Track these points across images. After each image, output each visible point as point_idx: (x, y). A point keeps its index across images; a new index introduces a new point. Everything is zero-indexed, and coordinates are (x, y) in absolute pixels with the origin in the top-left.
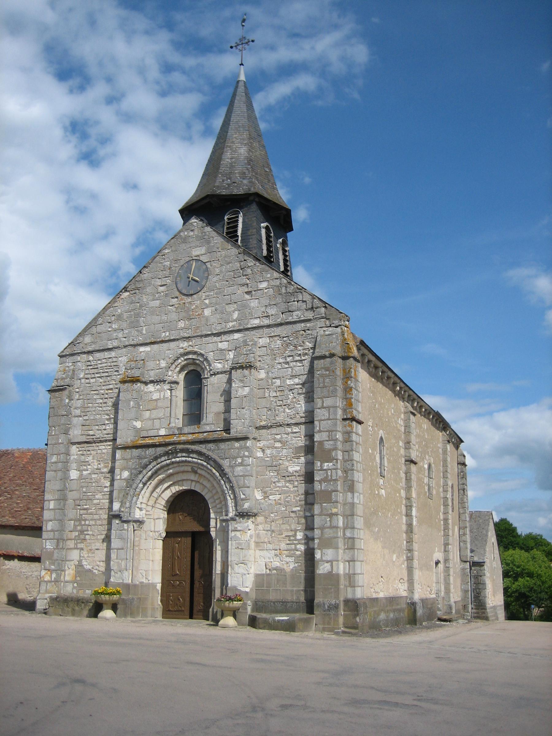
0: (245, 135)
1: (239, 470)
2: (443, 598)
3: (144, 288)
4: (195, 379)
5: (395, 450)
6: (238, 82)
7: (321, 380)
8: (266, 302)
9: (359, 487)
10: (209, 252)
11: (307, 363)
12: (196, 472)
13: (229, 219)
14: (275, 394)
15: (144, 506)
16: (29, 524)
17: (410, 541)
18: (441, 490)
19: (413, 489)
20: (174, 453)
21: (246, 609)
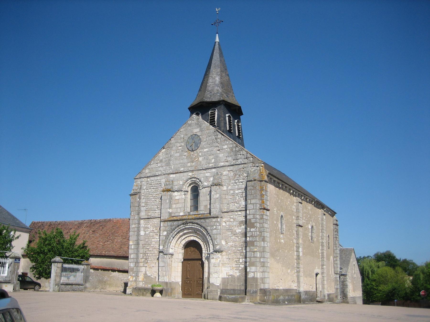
0: (219, 70)
1: (214, 231)
2: (321, 291)
3: (172, 147)
4: (195, 191)
5: (290, 220)
6: (215, 42)
7: (250, 191)
8: (227, 155)
9: (268, 239)
10: (201, 131)
11: (244, 183)
12: (196, 232)
13: (211, 113)
14: (230, 197)
15: (173, 247)
16: (122, 255)
17: (298, 263)
18: (320, 238)
19: (300, 239)
20: (186, 223)
21: (218, 293)
